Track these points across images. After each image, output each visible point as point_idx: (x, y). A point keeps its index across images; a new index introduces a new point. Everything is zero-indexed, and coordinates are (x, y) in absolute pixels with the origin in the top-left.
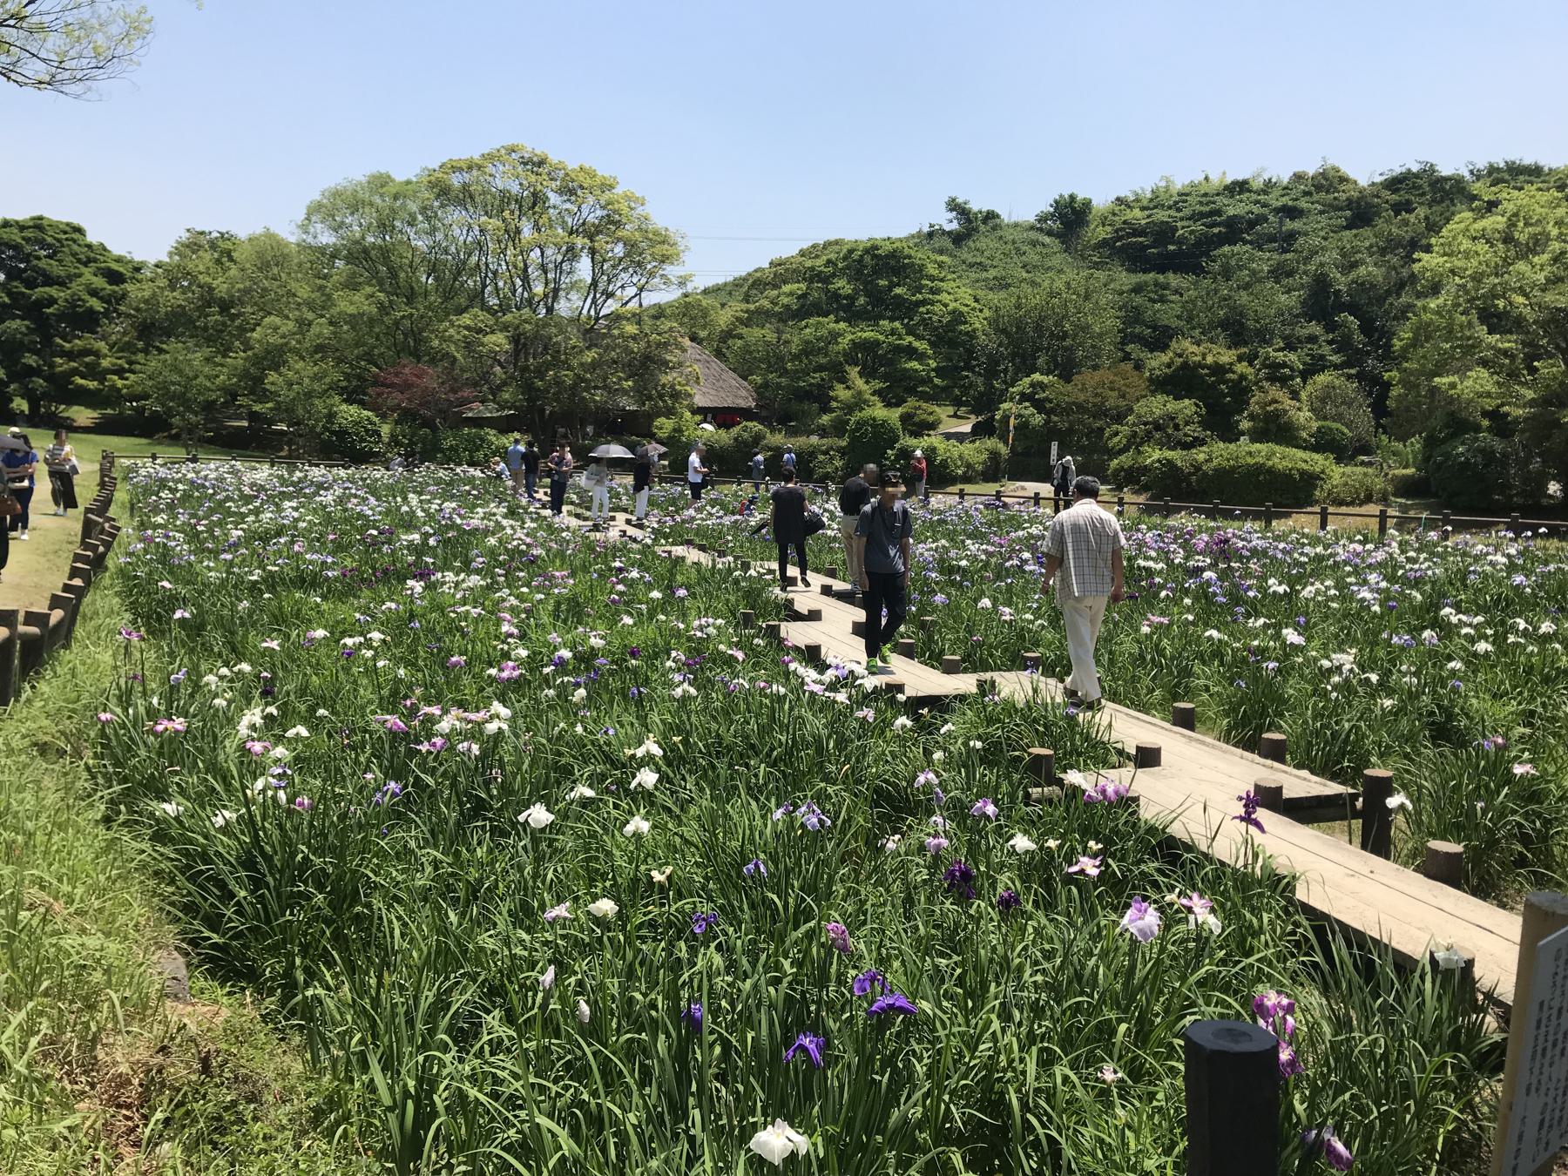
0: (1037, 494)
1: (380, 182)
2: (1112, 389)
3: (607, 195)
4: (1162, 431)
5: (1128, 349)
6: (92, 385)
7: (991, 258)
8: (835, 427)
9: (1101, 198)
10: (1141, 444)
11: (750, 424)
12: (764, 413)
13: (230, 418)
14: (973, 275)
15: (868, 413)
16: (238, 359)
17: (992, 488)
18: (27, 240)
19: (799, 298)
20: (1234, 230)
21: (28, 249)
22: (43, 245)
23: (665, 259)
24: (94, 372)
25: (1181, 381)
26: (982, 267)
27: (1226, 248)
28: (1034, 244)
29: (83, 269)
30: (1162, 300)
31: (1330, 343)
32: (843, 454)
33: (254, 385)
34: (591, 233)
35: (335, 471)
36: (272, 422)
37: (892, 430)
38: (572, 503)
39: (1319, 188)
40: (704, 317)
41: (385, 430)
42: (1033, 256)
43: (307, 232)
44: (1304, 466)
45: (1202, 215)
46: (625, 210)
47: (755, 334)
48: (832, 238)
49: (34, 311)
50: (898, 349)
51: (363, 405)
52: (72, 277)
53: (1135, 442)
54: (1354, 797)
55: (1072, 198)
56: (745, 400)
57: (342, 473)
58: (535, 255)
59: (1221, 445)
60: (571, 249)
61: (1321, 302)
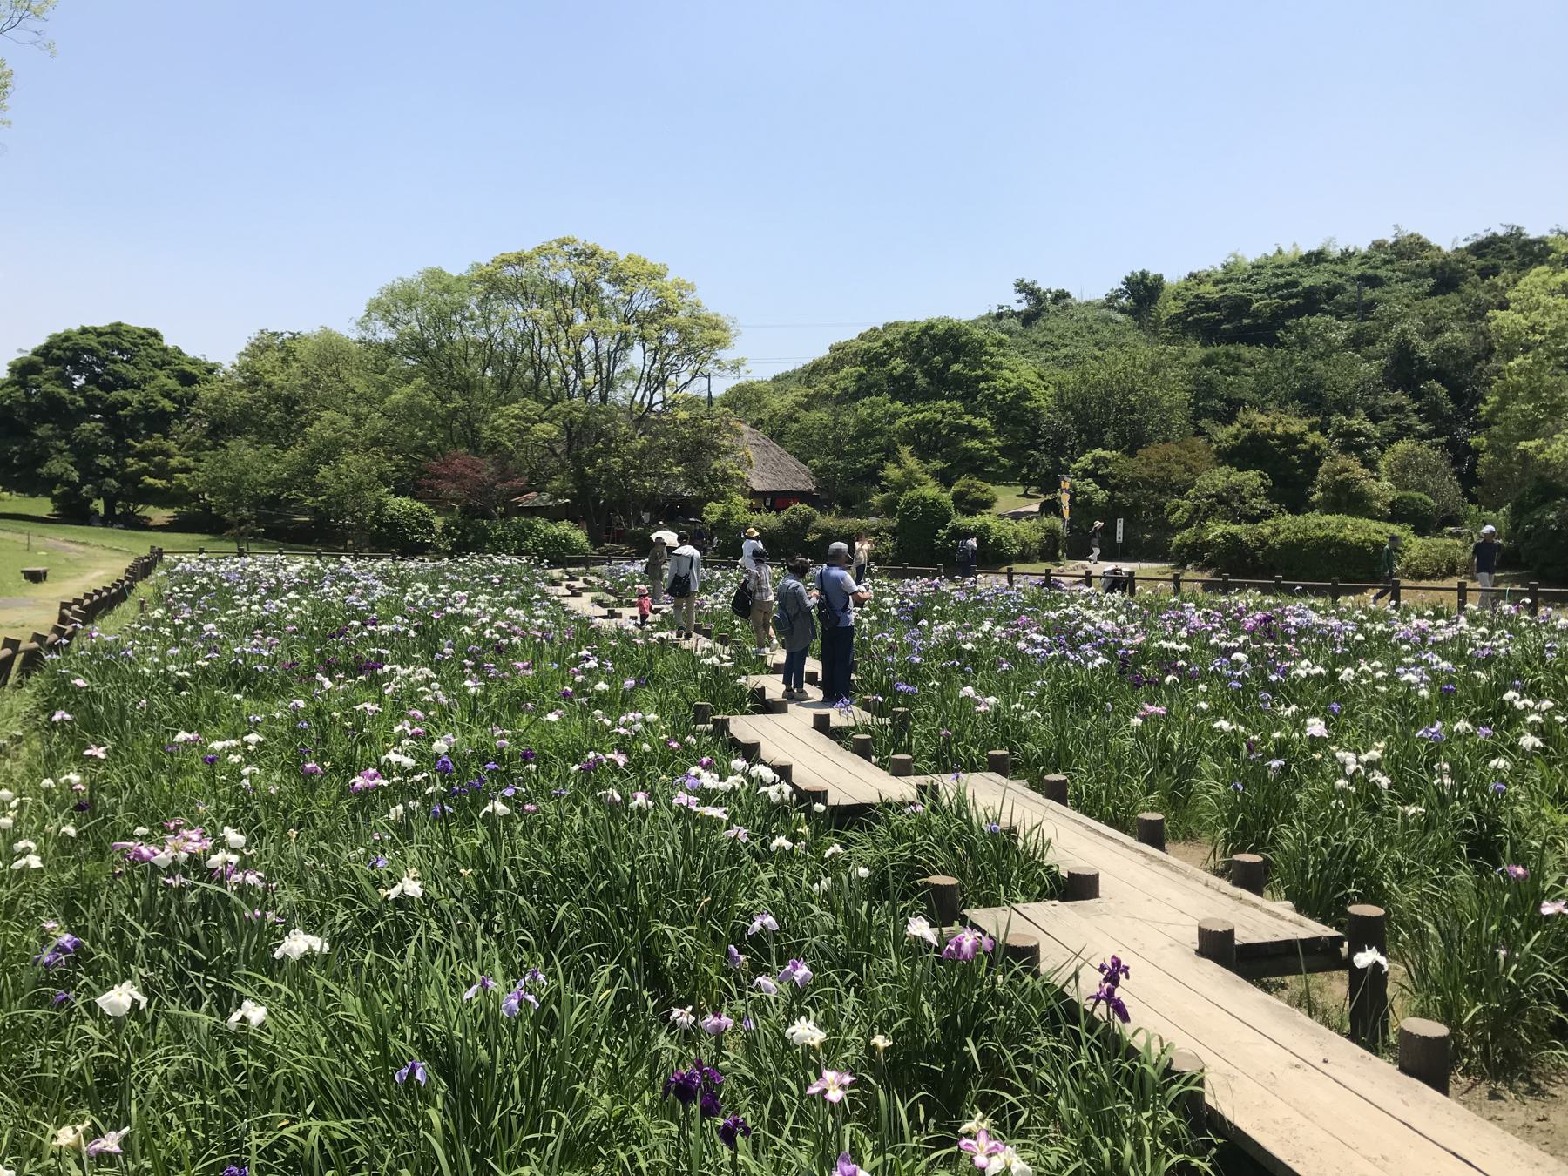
0: (1088, 572)
1: (435, 275)
2: (1178, 463)
3: (658, 282)
4: (1226, 503)
6: (160, 483)
9: (1173, 274)
10: (1206, 518)
11: (799, 506)
12: (825, 496)
15: (919, 491)
16: (293, 454)
17: (1041, 567)
18: (105, 344)
20: (1312, 302)
23: (715, 343)
24: (162, 472)
28: (1107, 321)
29: (158, 372)
30: (1235, 373)
31: (1417, 412)
32: (894, 534)
34: (643, 320)
37: (943, 509)
39: (1400, 255)
40: (759, 400)
41: (438, 522)
43: (367, 329)
45: (1277, 287)
47: (821, 415)
50: (960, 429)
52: (145, 381)
53: (1199, 516)
55: (1144, 274)
56: (806, 484)
58: (589, 344)
59: (1289, 517)
60: (625, 337)
61: (1404, 370)
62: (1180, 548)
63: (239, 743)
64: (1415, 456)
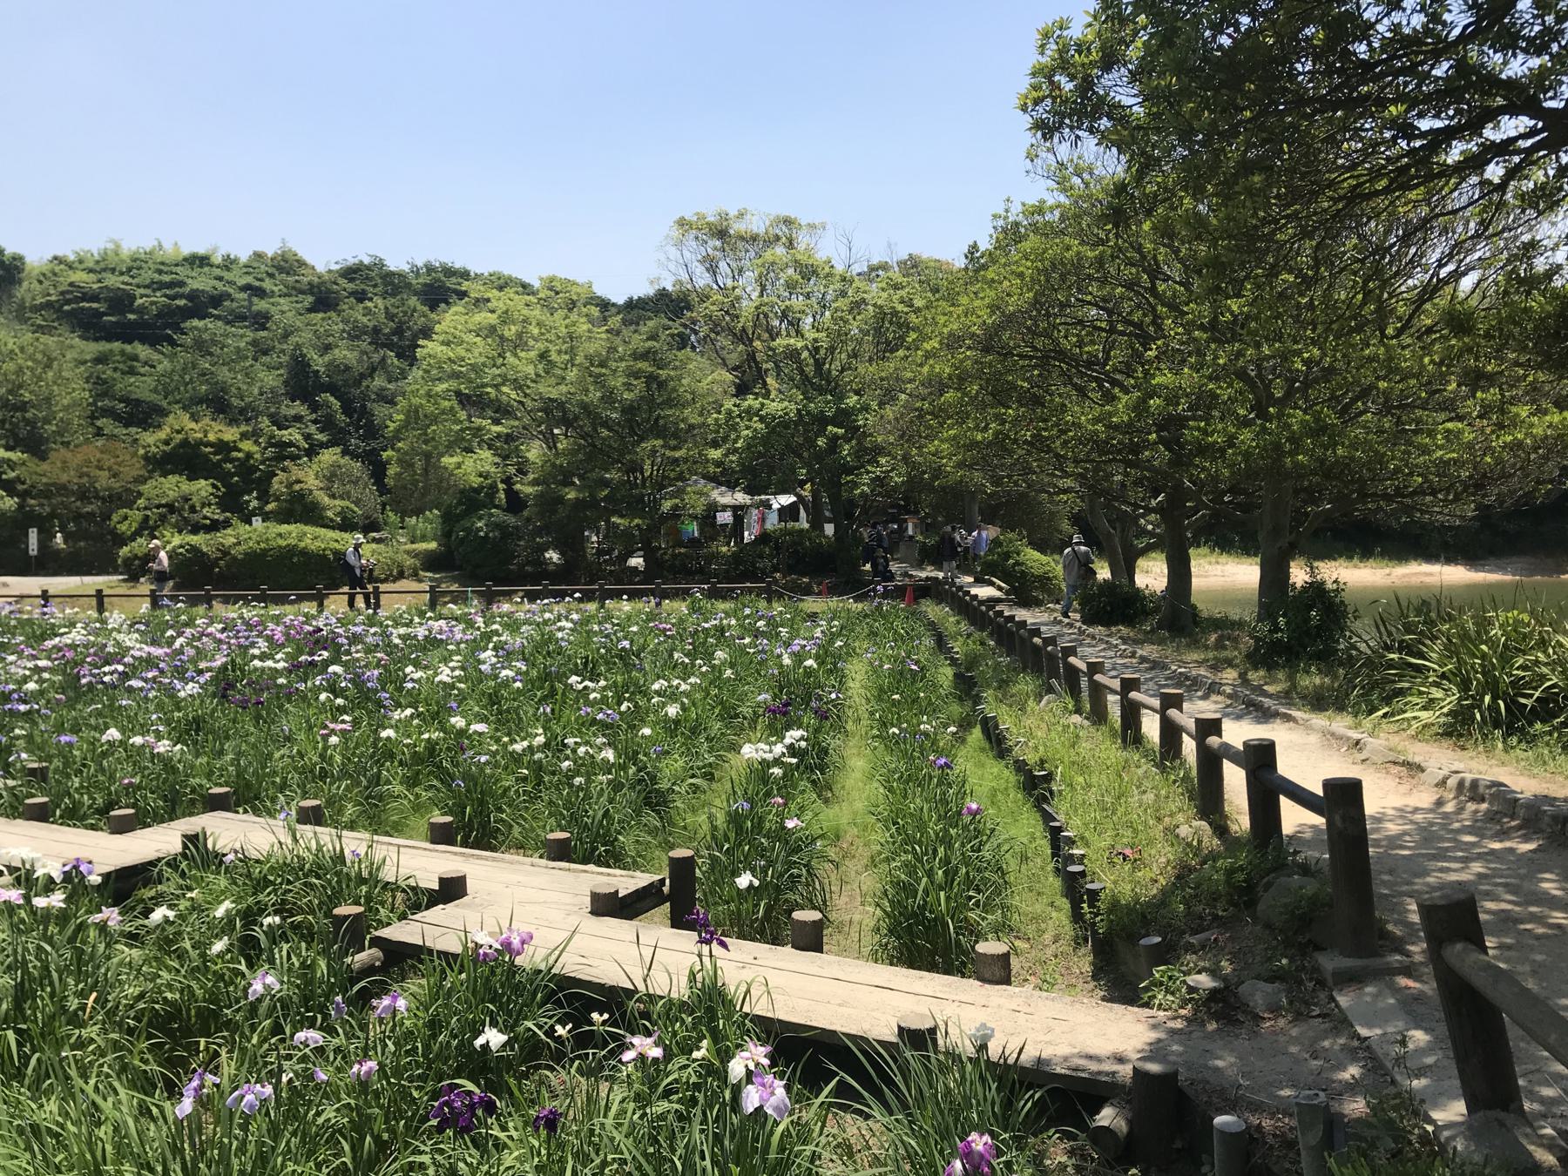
0: (45, 592)
2: (101, 468)
4: (178, 514)
5: (99, 423)
20: (201, 305)
25: (185, 459)
30: (132, 372)
31: (315, 422)
45: (162, 285)
53: (147, 528)
54: (662, 881)
62: (128, 562)
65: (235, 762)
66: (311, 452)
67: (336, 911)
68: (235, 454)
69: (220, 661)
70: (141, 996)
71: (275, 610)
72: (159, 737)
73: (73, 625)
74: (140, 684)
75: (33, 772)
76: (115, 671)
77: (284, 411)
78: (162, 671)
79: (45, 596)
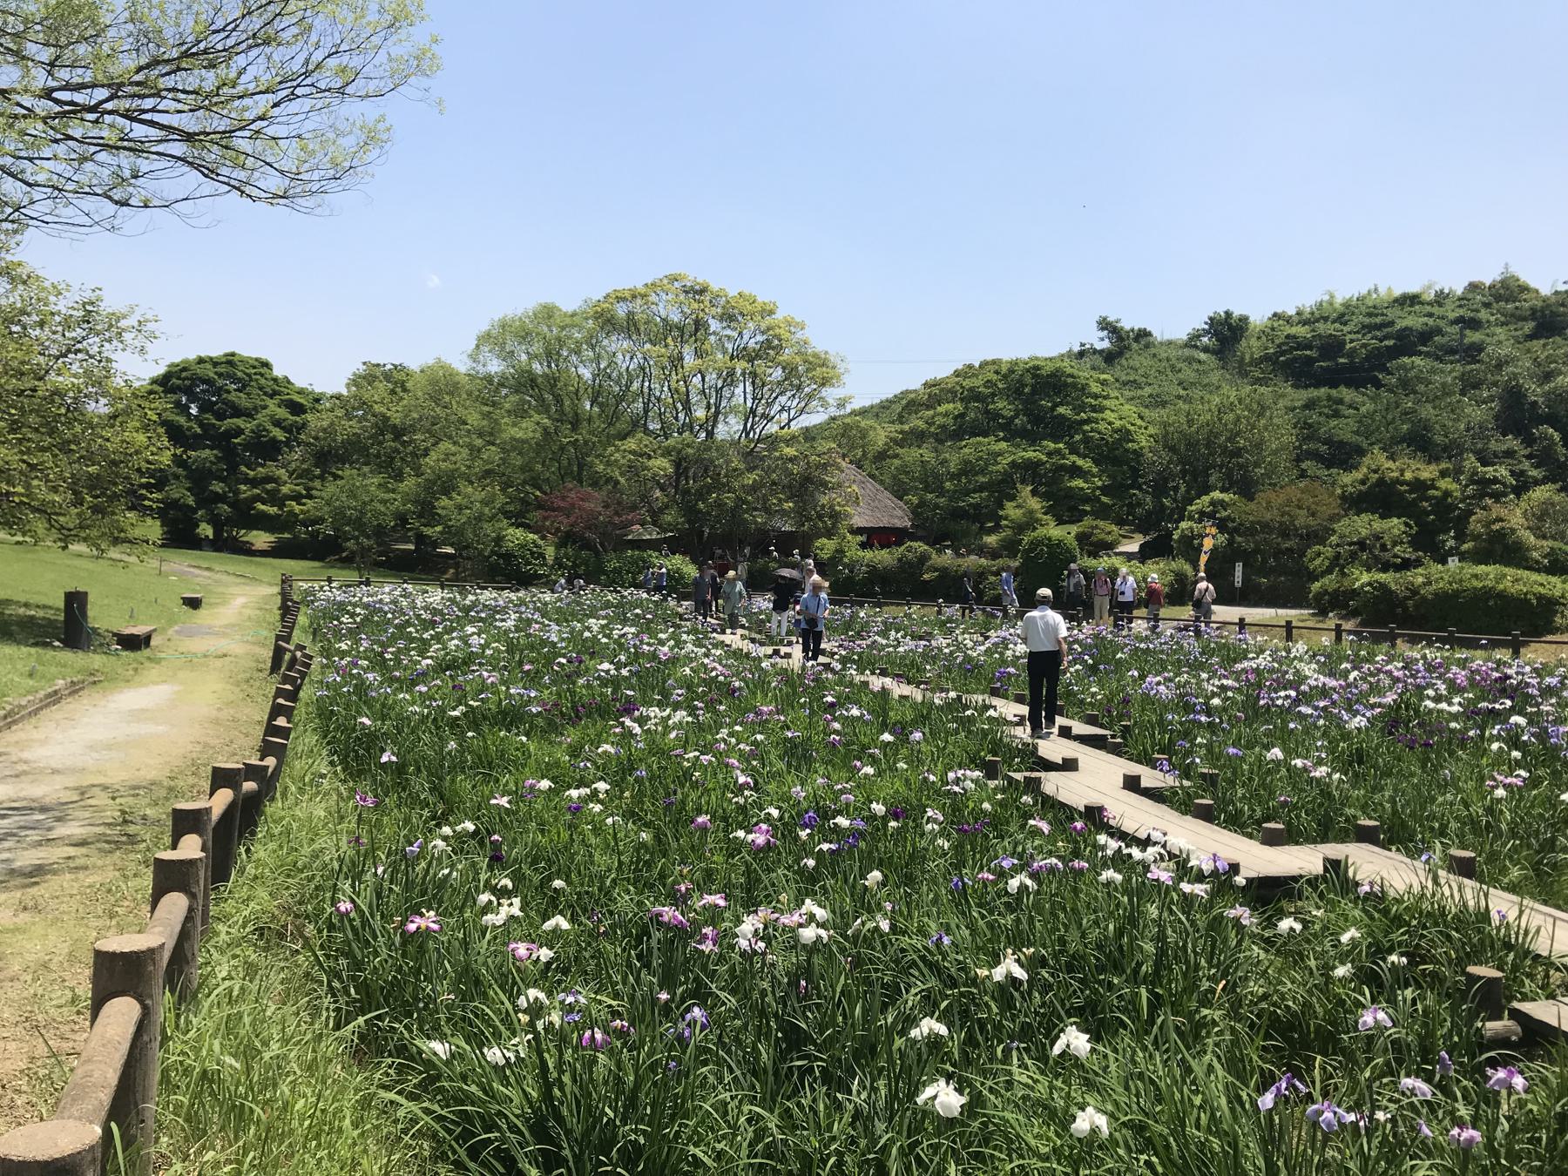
1: (547, 313)
2: (1300, 508)
3: (768, 321)
4: (1369, 551)
5: (1304, 466)
6: (273, 510)
7: (1146, 376)
8: (1004, 547)
9: (1258, 316)
13: (397, 541)
14: (1126, 393)
15: (1041, 532)
16: (409, 484)
18: (220, 375)
19: (956, 418)
20: (1408, 342)
21: (220, 382)
22: (236, 380)
23: (824, 382)
24: (275, 499)
25: (1381, 498)
26: (1135, 384)
27: (1406, 360)
28: (1190, 360)
31: (1529, 457)
33: (427, 511)
35: (506, 593)
36: (435, 545)
37: (1068, 551)
38: (743, 627)
39: (1498, 298)
41: (550, 552)
42: (1188, 374)
44: (1541, 589)
46: (785, 335)
47: (912, 454)
48: (989, 358)
49: (222, 441)
51: (527, 527)
55: (1228, 314)
57: (513, 596)
60: (732, 373)
62: (1319, 596)
63: (588, 791)
64: (1553, 504)
65: (1392, 801)
66: (1522, 486)
67: (1471, 969)
68: (1432, 492)
69: (1389, 699)
70: (1265, 997)
71: (1461, 654)
72: (1320, 762)
73: (1262, 651)
74: (1310, 711)
75: (1203, 776)
76: (1287, 697)
77: (1493, 446)
78: (1334, 703)
79: (1242, 624)
